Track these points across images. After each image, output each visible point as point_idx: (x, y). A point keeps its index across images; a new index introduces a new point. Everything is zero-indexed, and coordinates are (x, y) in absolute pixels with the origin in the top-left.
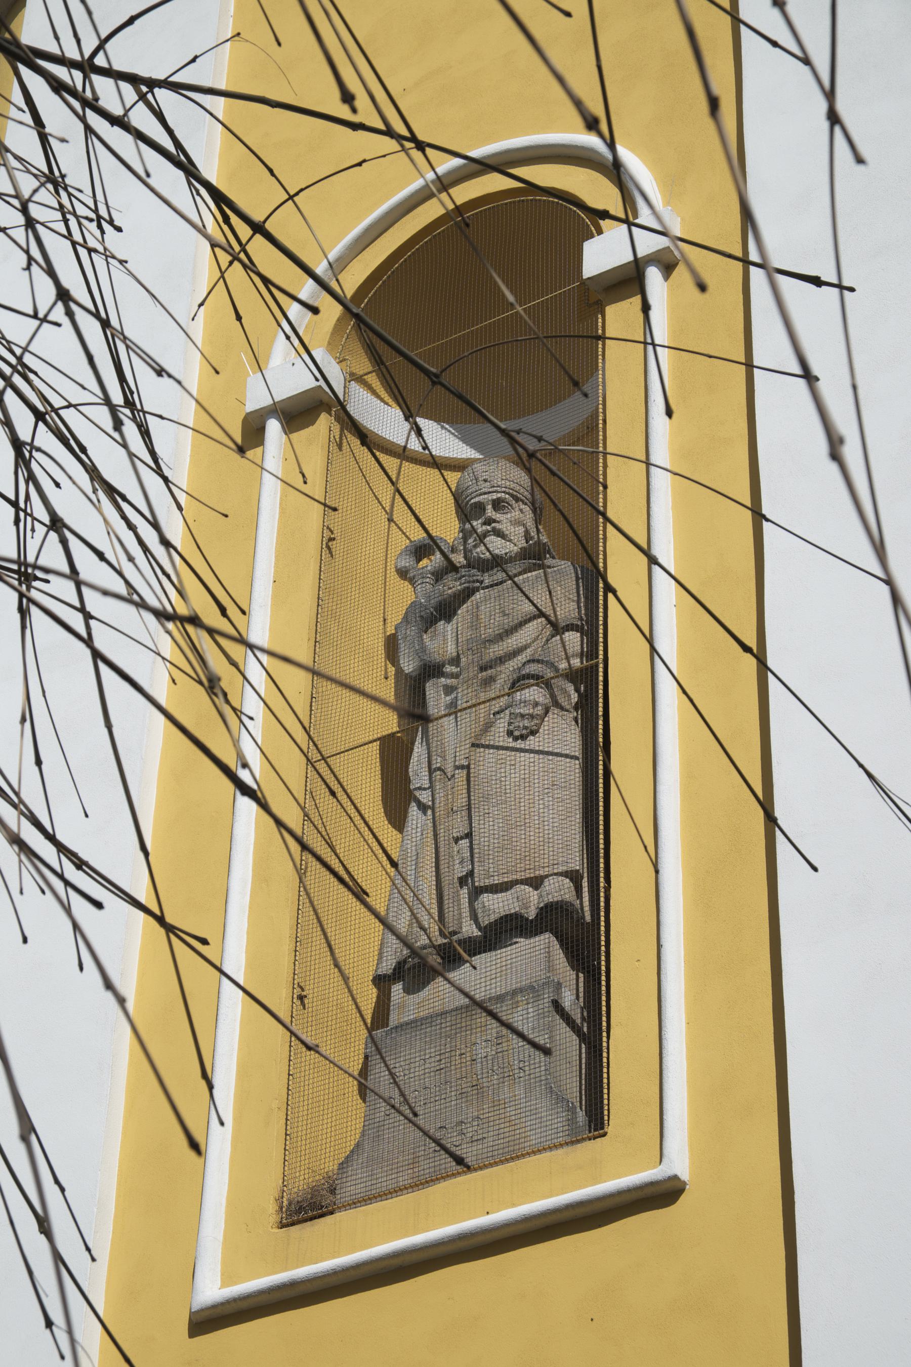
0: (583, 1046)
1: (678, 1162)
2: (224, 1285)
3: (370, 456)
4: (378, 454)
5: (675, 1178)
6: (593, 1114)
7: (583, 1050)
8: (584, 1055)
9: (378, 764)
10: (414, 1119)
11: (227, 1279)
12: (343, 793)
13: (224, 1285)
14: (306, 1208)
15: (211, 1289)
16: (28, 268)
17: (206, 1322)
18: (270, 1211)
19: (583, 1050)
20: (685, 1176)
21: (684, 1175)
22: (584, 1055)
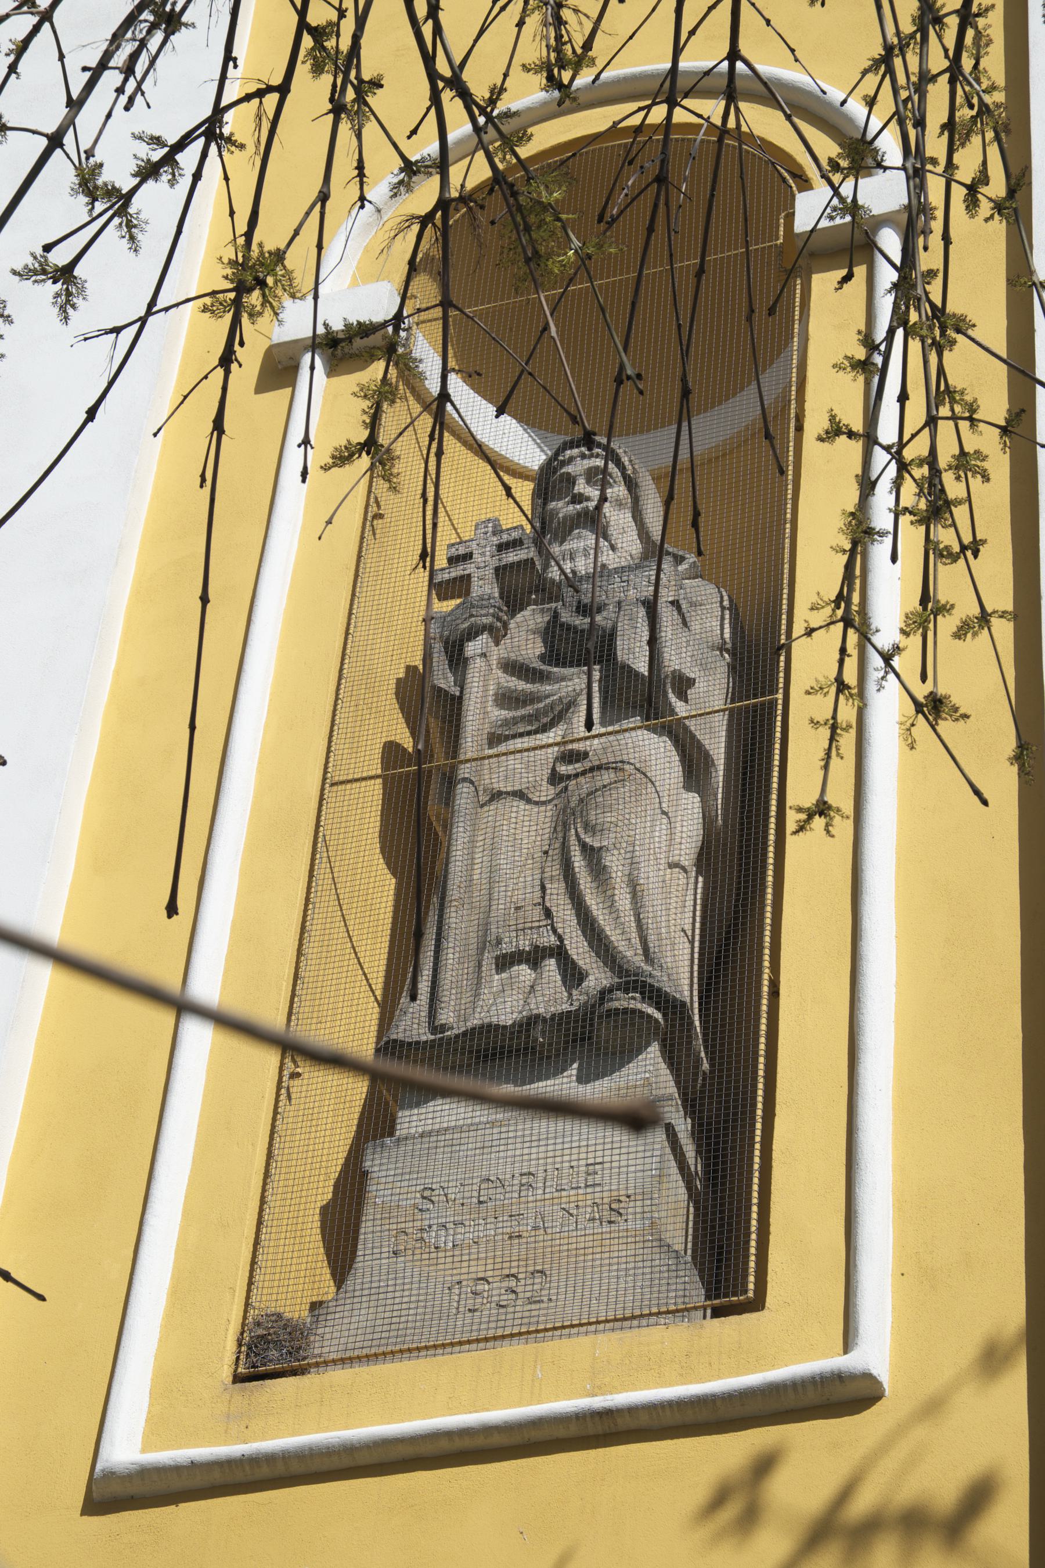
0: (700, 879)
1: (874, 1354)
2: (143, 1451)
3: (493, 475)
4: (502, 474)
5: (868, 1377)
6: (725, 1265)
7: (700, 885)
8: (698, 913)
9: (391, 898)
10: (587, 764)
11: (156, 1430)
12: (688, 441)
13: (143, 1451)
14: (270, 1353)
15: (126, 1449)
16: (919, 495)
17: (112, 1495)
18: (224, 1354)
19: (700, 885)
20: (884, 1377)
21: (882, 1372)
22: (698, 913)
